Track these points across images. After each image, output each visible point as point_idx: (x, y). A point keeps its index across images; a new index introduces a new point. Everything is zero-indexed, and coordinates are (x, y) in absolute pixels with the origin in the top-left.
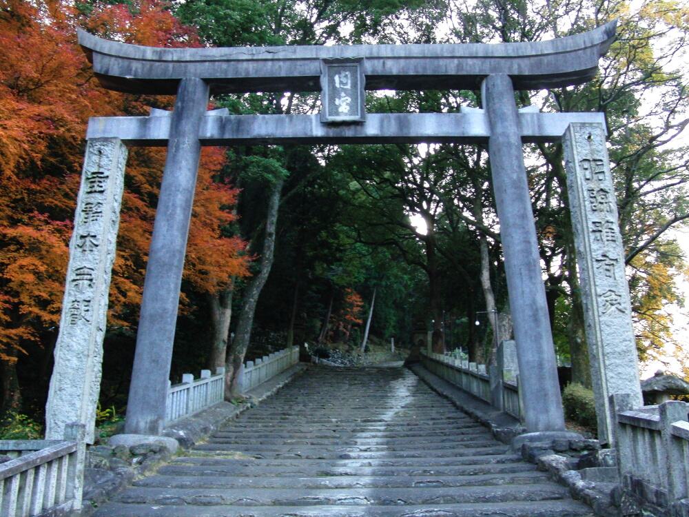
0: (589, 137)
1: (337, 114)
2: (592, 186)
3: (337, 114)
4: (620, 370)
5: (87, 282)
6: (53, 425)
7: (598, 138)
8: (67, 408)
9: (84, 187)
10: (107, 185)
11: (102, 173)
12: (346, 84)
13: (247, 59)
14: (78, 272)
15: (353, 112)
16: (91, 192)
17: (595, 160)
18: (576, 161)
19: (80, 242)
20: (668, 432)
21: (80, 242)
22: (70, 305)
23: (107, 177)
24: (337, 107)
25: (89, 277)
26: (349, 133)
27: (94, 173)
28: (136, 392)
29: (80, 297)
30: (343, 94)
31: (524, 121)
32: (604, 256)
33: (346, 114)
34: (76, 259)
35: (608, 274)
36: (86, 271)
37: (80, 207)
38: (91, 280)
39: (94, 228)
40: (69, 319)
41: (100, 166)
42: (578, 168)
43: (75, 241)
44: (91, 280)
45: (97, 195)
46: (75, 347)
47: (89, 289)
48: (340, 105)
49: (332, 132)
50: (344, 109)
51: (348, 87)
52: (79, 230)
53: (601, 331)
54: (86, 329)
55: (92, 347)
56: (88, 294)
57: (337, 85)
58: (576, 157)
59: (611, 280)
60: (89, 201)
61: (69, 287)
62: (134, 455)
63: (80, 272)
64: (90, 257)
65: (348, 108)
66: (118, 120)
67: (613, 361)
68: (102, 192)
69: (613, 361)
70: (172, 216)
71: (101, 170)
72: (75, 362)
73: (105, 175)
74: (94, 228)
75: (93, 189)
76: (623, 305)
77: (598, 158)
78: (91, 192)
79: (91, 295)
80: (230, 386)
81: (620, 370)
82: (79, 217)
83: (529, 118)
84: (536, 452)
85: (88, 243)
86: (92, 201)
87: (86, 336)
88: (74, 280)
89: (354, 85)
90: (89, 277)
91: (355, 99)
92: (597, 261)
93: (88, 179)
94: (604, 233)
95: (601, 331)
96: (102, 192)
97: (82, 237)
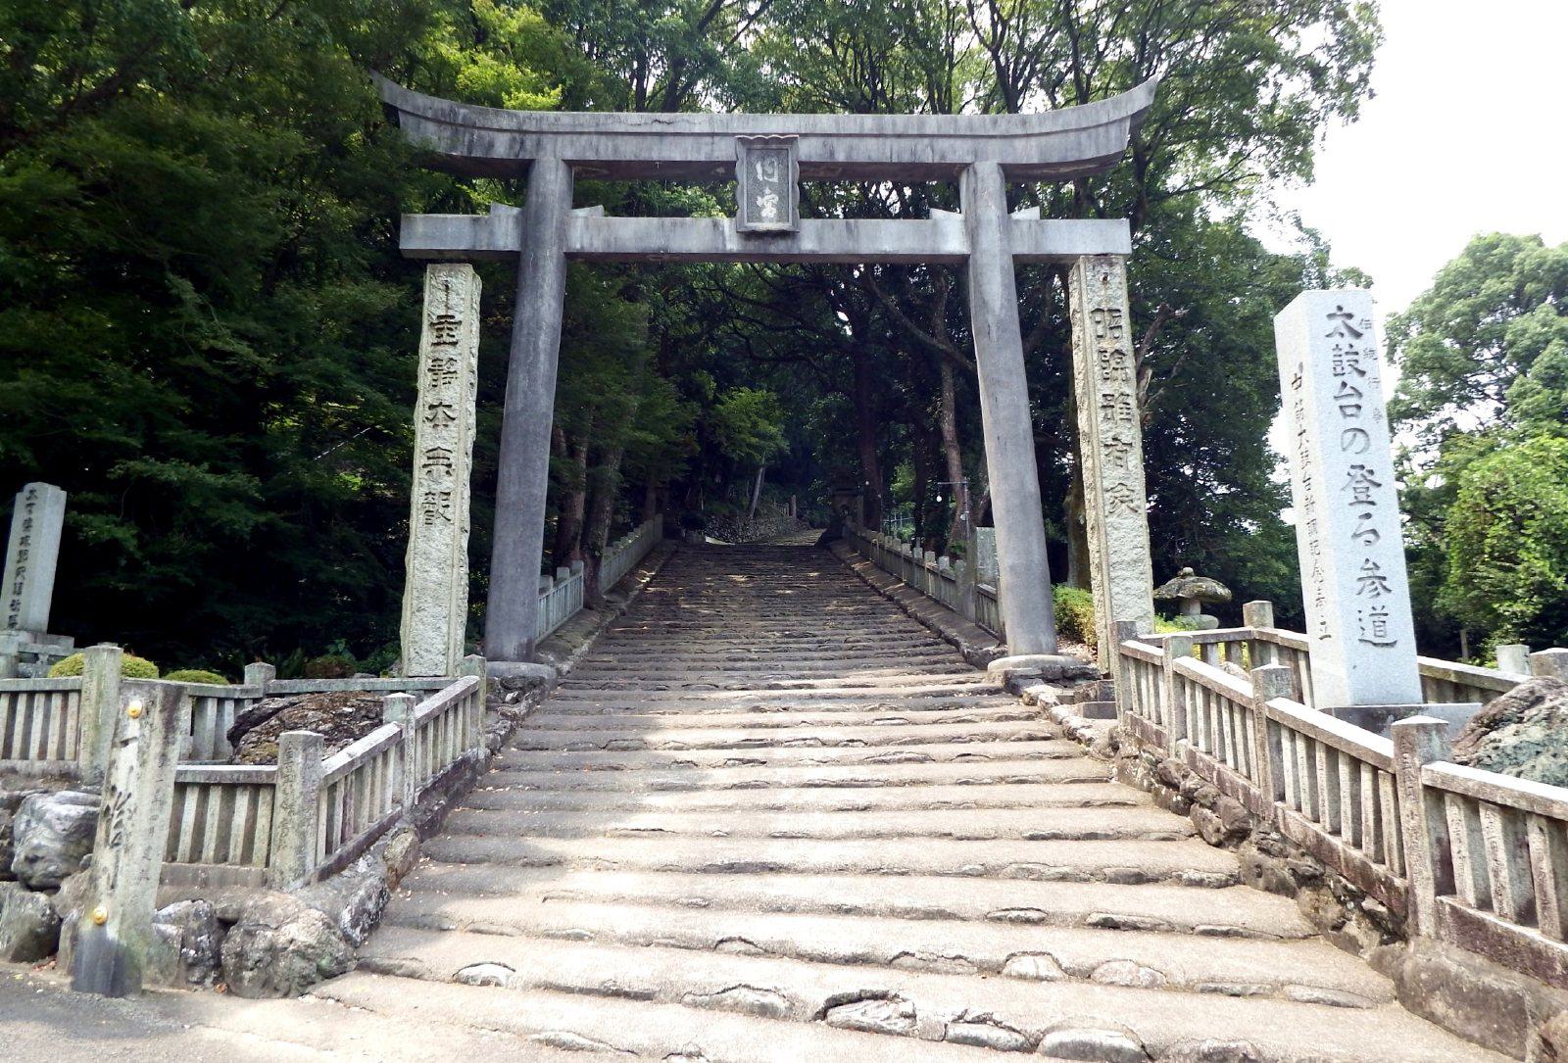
0: (1105, 279)
1: (760, 219)
2: (1105, 344)
3: (760, 219)
4: (1128, 584)
5: (444, 469)
6: (413, 655)
7: (1118, 280)
8: (432, 634)
9: (427, 337)
10: (460, 333)
11: (452, 317)
12: (772, 175)
13: (628, 134)
14: (431, 454)
15: (780, 218)
16: (438, 344)
17: (1110, 311)
18: (1086, 312)
19: (429, 413)
20: (1169, 670)
21: (429, 413)
22: (422, 500)
23: (460, 322)
24: (760, 209)
25: (446, 462)
26: (778, 247)
27: (439, 317)
28: (498, 607)
29: (437, 488)
30: (767, 191)
31: (1017, 232)
32: (1115, 439)
33: (771, 220)
34: (425, 437)
35: (1119, 462)
36: (441, 453)
37: (425, 364)
38: (449, 466)
39: (448, 394)
40: (422, 517)
41: (448, 307)
42: (1088, 321)
43: (421, 412)
44: (449, 466)
45: (447, 347)
46: (435, 555)
47: (446, 478)
48: (763, 206)
49: (752, 246)
50: (769, 213)
51: (775, 179)
52: (425, 397)
53: (1107, 535)
54: (446, 531)
55: (456, 554)
56: (447, 484)
57: (760, 177)
58: (1085, 305)
59: (1122, 471)
60: (437, 355)
61: (418, 474)
62: (508, 689)
63: (433, 454)
64: (445, 433)
65: (775, 210)
66: (445, 219)
67: (1119, 573)
68: (454, 344)
69: (1119, 573)
70: (534, 364)
71: (450, 313)
72: (435, 574)
73: (457, 319)
74: (448, 394)
75: (441, 340)
76: (1136, 503)
77: (1115, 307)
78: (438, 344)
79: (451, 485)
80: (592, 579)
81: (1128, 584)
82: (424, 380)
83: (1025, 227)
84: (1021, 681)
85: (441, 416)
86: (441, 356)
87: (449, 541)
88: (425, 466)
89: (784, 177)
90: (446, 462)
91: (783, 198)
92: (1106, 446)
93: (432, 324)
94: (1117, 409)
95: (1107, 535)
96: (454, 344)
97: (432, 407)
